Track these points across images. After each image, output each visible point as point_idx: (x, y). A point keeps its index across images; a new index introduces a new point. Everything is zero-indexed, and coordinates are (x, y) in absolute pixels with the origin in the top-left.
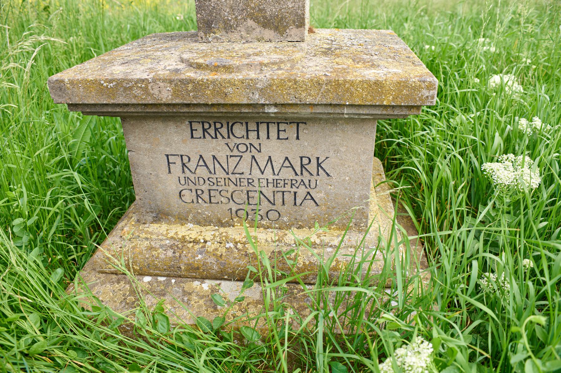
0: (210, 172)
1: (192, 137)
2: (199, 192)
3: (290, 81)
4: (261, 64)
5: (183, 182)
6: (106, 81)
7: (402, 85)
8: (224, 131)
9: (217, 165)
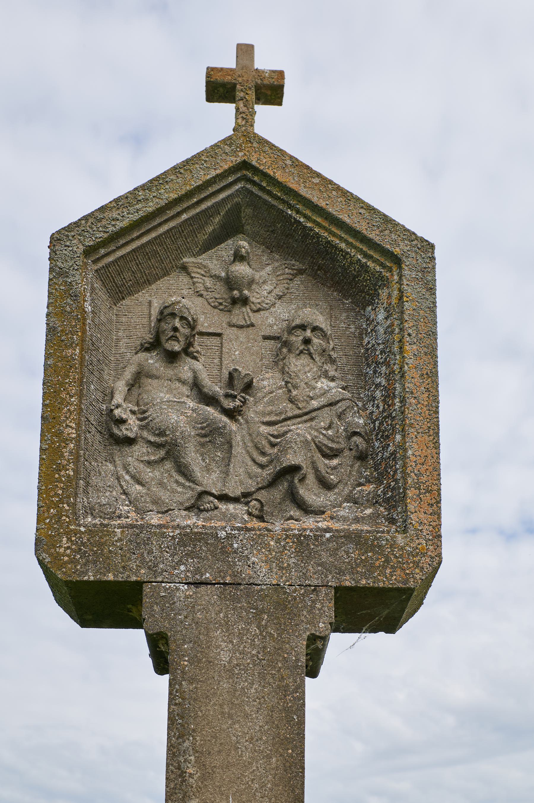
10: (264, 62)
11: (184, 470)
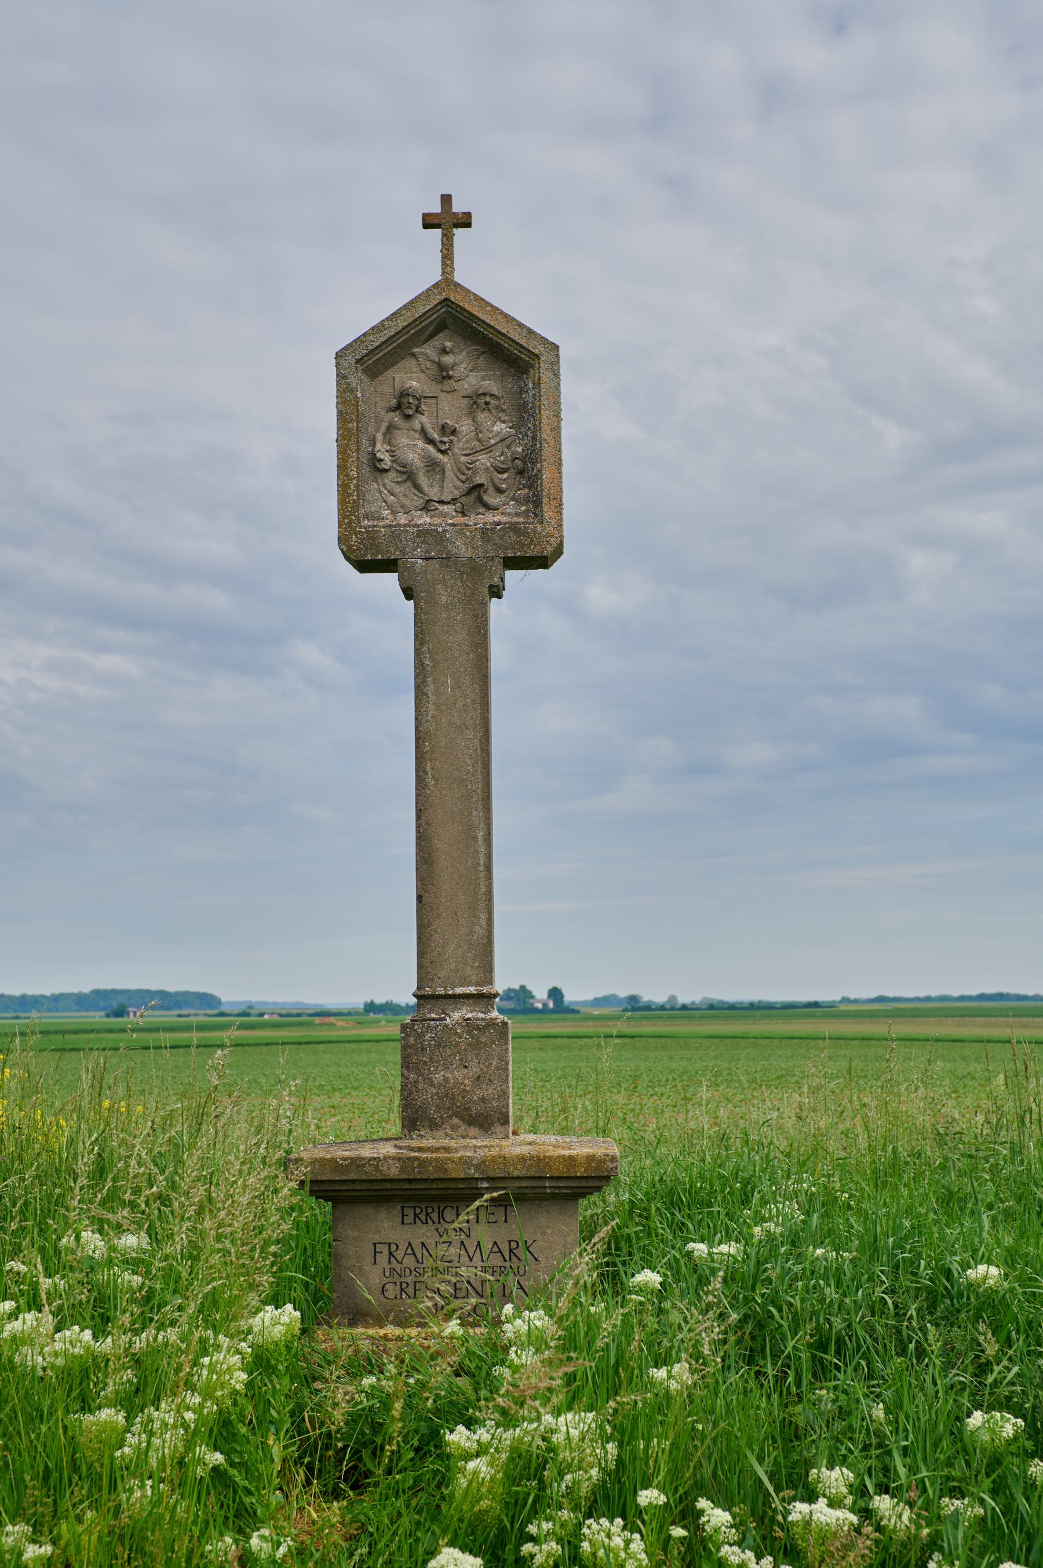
0: (418, 1262)
1: (403, 1223)
2: (404, 1285)
3: (500, 1157)
4: (475, 1146)
5: (387, 1274)
6: (342, 1159)
7: (590, 1158)
8: (435, 1216)
9: (426, 1253)
10: (457, 207)
11: (417, 487)
